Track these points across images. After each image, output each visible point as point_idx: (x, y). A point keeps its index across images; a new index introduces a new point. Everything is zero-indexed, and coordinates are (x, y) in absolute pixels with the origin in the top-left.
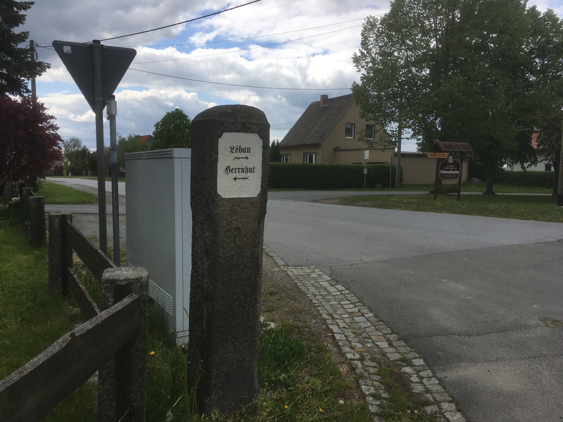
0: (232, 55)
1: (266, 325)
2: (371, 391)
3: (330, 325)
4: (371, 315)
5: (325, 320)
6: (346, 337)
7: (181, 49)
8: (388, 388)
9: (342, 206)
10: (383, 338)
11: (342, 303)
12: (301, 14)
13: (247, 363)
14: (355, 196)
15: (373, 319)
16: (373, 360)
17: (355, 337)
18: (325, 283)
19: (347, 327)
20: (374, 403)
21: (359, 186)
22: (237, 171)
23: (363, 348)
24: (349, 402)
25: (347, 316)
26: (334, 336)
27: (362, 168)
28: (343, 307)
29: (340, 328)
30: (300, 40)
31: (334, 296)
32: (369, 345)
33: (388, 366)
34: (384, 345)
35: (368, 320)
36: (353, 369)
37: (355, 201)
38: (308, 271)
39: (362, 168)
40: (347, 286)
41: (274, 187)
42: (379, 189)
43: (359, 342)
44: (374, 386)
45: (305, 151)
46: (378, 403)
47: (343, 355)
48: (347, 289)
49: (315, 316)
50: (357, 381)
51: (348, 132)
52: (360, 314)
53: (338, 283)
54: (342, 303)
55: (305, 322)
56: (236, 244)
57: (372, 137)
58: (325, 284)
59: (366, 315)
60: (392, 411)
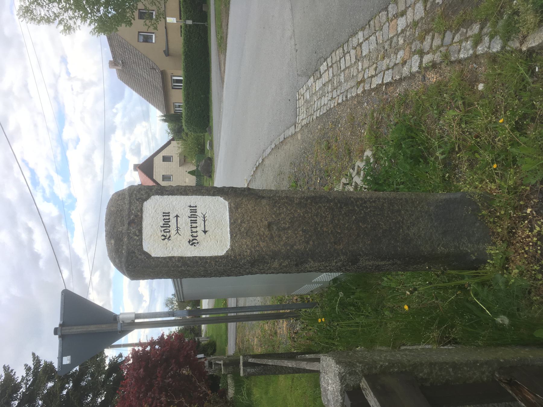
0: (76, 158)
1: (368, 159)
2: (469, 47)
3: (372, 87)
4: (360, 34)
5: (364, 92)
6: (388, 69)
7: (72, 207)
8: (466, 23)
9: (227, 51)
10: (393, 23)
11: (343, 67)
12: (25, 86)
13: (432, 208)
14: (217, 36)
15: (366, 32)
16: (422, 39)
17: (389, 57)
18: (317, 84)
19: (375, 65)
20: (487, 45)
21: (205, 31)
22: (194, 230)
23: (404, 50)
24: (483, 78)
25: (360, 64)
26: (387, 84)
27: (186, 25)
28: (348, 67)
29: (376, 75)
30: (55, 87)
31: (334, 76)
32: (401, 41)
33: (433, 20)
34: (402, 23)
35: (367, 39)
36: (434, 65)
37: (221, 37)
38: (302, 102)
39: (186, 25)
40: (323, 60)
41: (209, 121)
42: (208, 7)
43: (397, 54)
44: (460, 42)
45: (171, 88)
46: (487, 39)
47: (412, 76)
48: (325, 60)
49: (359, 102)
50: (452, 62)
51: (147, 39)
52: (358, 48)
53: (317, 70)
54: (343, 67)
55: (366, 115)
56: (289, 227)
57: (152, 13)
58: (319, 84)
59: (361, 41)
60: (501, 23)
